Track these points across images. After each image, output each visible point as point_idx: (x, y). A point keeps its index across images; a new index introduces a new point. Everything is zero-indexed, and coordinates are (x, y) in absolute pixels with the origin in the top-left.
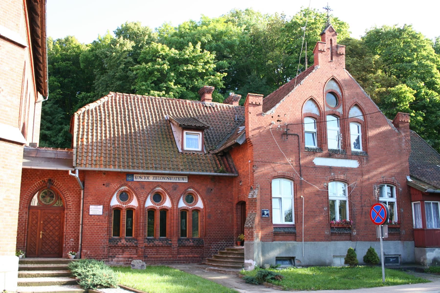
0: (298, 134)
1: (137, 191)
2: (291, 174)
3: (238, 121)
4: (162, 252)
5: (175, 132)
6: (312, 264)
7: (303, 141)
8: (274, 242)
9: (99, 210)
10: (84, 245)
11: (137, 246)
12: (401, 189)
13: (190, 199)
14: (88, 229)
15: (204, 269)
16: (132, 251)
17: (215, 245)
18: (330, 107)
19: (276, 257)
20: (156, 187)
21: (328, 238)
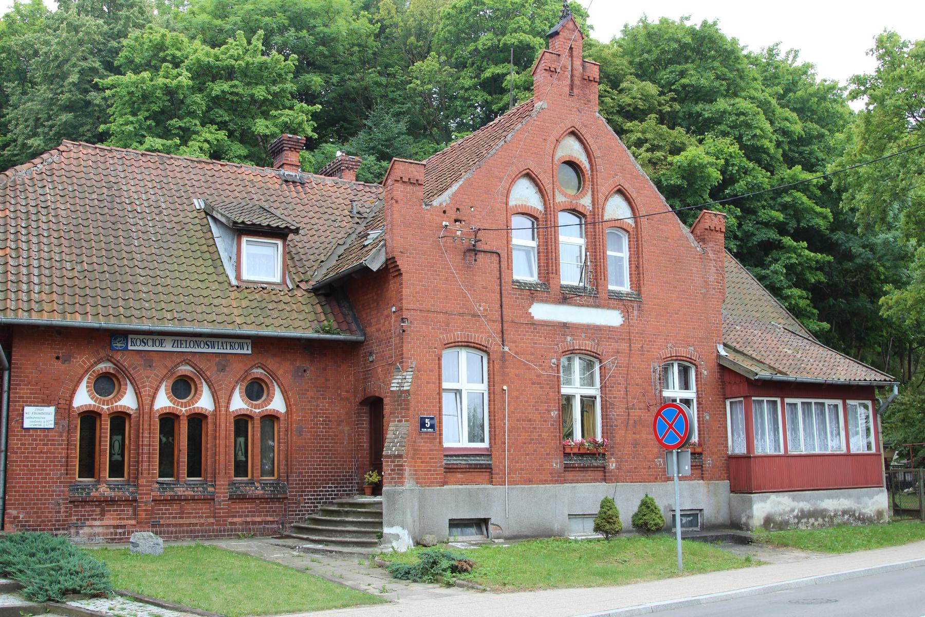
0: (498, 251)
1: (136, 372)
2: (482, 338)
3: (359, 216)
4: (192, 513)
5: (220, 239)
6: (525, 533)
7: (509, 267)
8: (445, 487)
9: (47, 416)
10: (11, 500)
11: (135, 500)
12: (705, 373)
13: (255, 390)
14: (21, 461)
15: (292, 548)
16: (124, 511)
17: (312, 495)
18: (565, 195)
19: (450, 520)
20: (179, 364)
21: (558, 477)
